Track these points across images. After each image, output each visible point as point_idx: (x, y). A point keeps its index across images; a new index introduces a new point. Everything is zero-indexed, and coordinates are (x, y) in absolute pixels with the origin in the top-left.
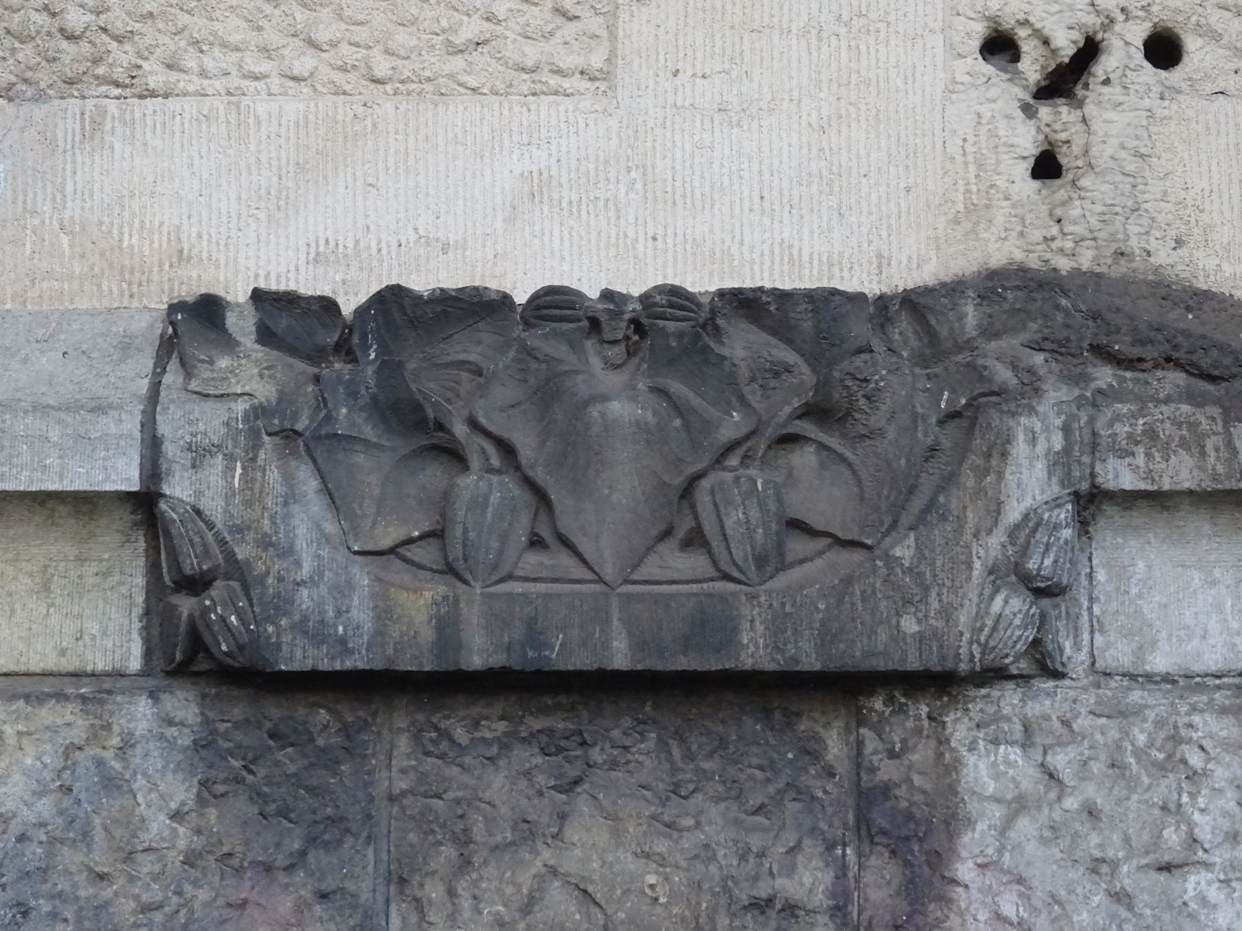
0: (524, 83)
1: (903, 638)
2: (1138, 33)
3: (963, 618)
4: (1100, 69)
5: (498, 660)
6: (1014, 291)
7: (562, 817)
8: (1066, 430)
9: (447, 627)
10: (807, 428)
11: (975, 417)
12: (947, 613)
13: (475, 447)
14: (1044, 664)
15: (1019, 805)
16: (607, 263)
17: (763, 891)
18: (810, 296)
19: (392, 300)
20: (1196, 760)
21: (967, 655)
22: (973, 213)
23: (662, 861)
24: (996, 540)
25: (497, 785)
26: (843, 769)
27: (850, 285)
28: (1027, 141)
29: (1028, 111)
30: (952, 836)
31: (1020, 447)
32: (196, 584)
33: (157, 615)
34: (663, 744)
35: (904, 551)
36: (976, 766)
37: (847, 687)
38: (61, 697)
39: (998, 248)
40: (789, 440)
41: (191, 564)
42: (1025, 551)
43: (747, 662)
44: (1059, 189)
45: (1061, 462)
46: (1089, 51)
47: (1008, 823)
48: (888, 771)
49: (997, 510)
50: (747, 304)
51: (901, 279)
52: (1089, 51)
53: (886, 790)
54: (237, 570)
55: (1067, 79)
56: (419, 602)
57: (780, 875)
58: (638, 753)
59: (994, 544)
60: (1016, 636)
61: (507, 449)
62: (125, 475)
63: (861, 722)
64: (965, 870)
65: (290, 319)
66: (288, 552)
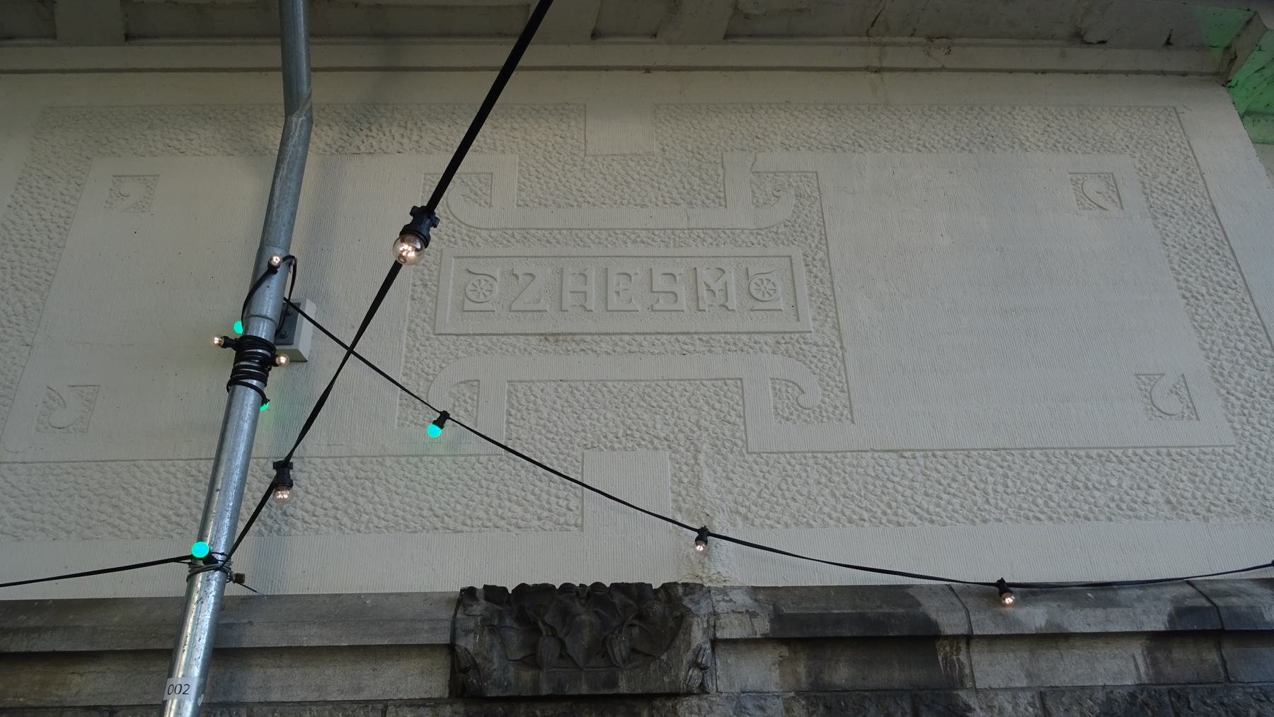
1: (665, 684)
9: (536, 683)
12: (677, 676)
14: (703, 689)
16: (583, 577)
18: (637, 585)
19: (522, 588)
21: (683, 688)
24: (690, 653)
31: (695, 628)
32: (465, 671)
35: (664, 657)
36: (958, 660)
38: (424, 706)
41: (463, 665)
42: (697, 656)
43: (621, 691)
54: (476, 666)
56: (527, 675)
59: (689, 656)
61: (553, 629)
62: (444, 638)
65: (493, 593)
66: (491, 661)
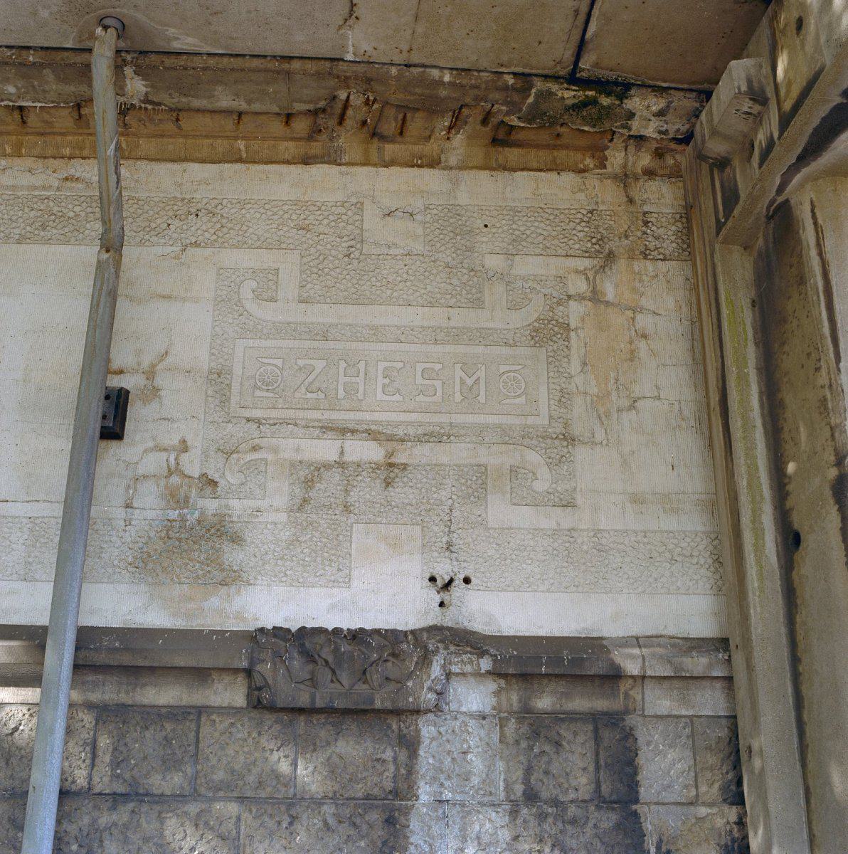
0: (331, 584)
2: (462, 577)
3: (422, 698)
4: (454, 584)
5: (323, 706)
6: (434, 630)
7: (336, 740)
8: (445, 659)
10: (390, 658)
11: (425, 660)
13: (320, 661)
15: (433, 739)
17: (379, 756)
20: (470, 730)
22: (426, 613)
23: (357, 750)
24: (430, 682)
25: (323, 733)
26: (396, 731)
27: (400, 629)
28: (438, 599)
29: (438, 592)
30: (419, 745)
31: (435, 663)
32: (259, 689)
33: (249, 696)
34: (358, 726)
37: (397, 713)
39: (430, 621)
40: (386, 661)
44: (444, 610)
45: (444, 667)
46: (451, 581)
47: (431, 743)
48: (405, 731)
49: (429, 676)
50: (377, 631)
51: (410, 627)
52: (451, 581)
53: (405, 735)
55: (448, 585)
57: (366, 813)
58: (351, 725)
60: (433, 702)
61: (326, 662)
62: (245, 664)
63: (400, 721)
64: (421, 752)
